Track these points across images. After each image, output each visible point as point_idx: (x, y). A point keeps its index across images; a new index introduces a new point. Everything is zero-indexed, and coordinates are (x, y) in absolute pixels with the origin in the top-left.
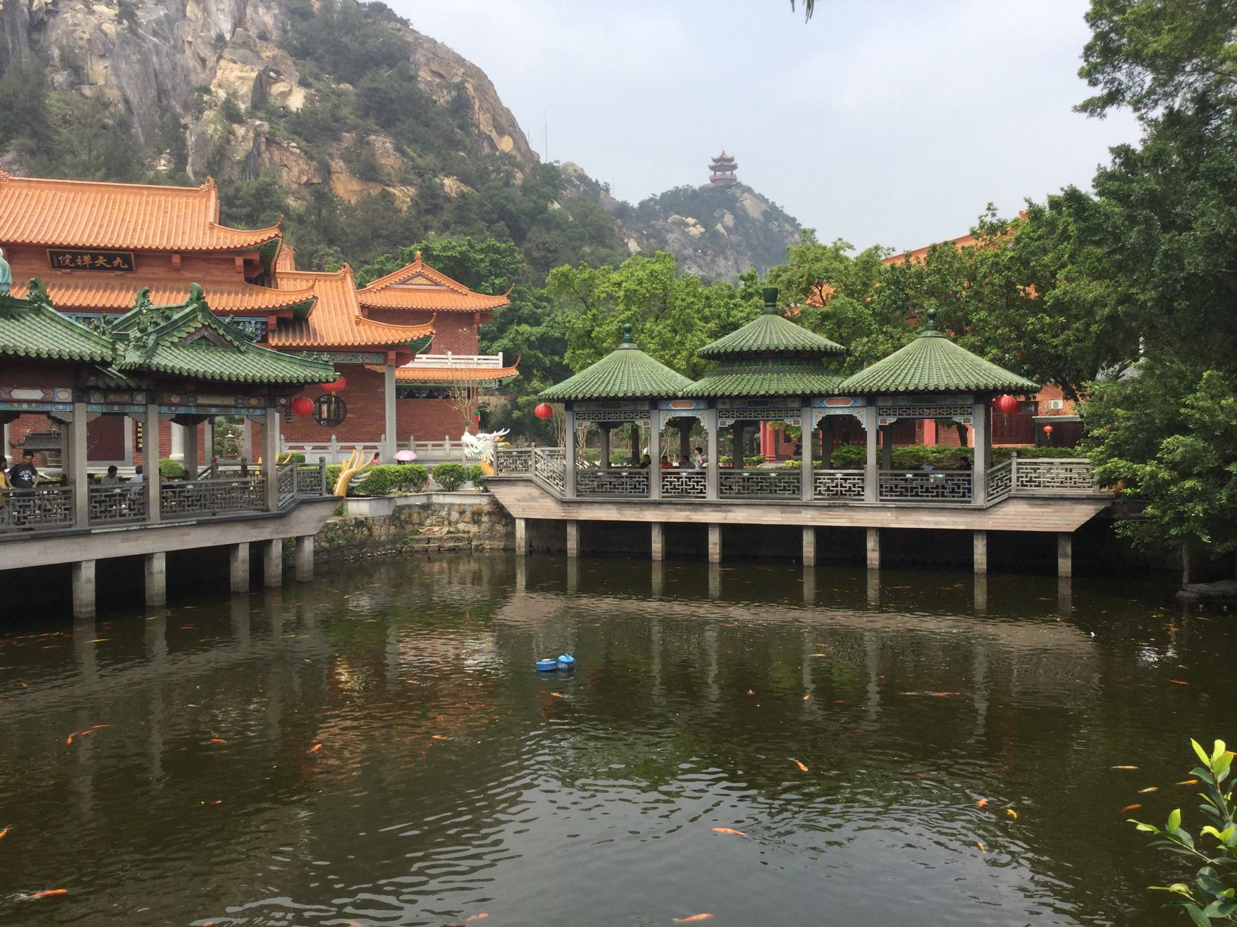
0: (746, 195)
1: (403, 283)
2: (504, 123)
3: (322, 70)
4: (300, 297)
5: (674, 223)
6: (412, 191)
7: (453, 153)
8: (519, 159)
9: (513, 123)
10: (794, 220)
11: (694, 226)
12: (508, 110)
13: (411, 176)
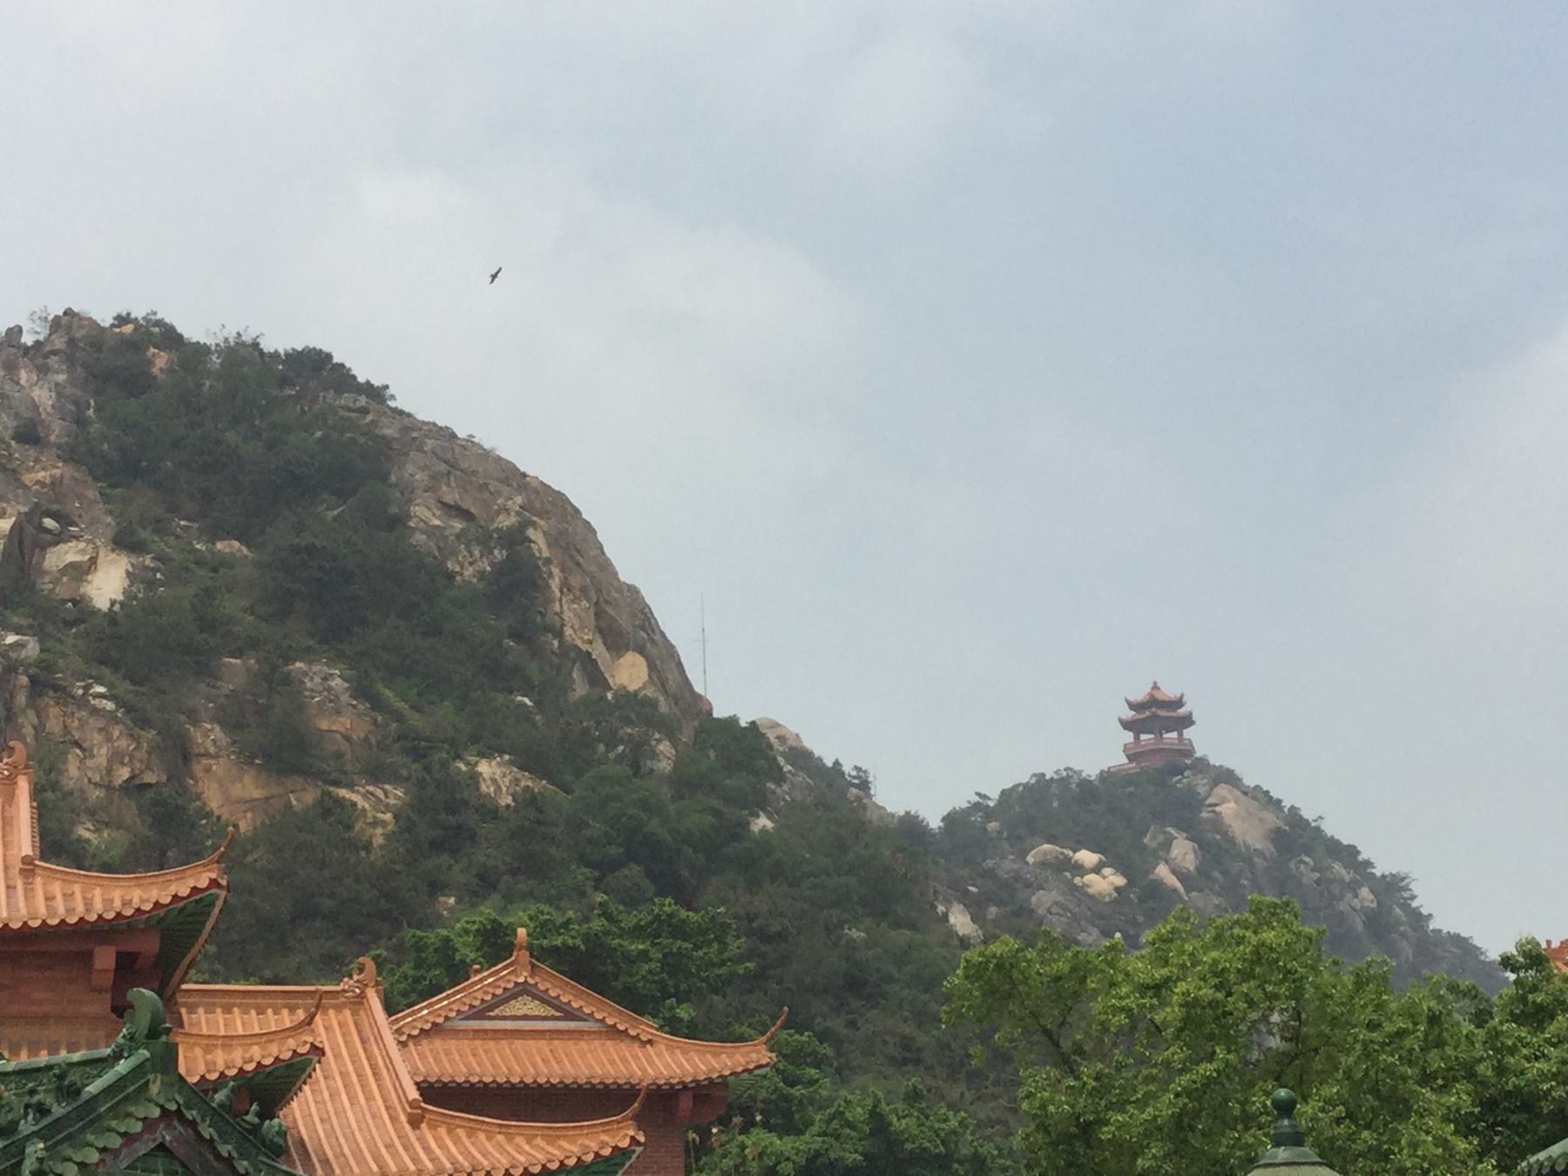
0: (1222, 790)
1: (480, 1014)
2: (625, 622)
3: (174, 509)
4: (274, 1049)
5: (1044, 864)
6: (396, 794)
7: (500, 698)
8: (663, 707)
9: (645, 619)
10: (1352, 851)
11: (1097, 870)
12: (633, 591)
13: (394, 758)
